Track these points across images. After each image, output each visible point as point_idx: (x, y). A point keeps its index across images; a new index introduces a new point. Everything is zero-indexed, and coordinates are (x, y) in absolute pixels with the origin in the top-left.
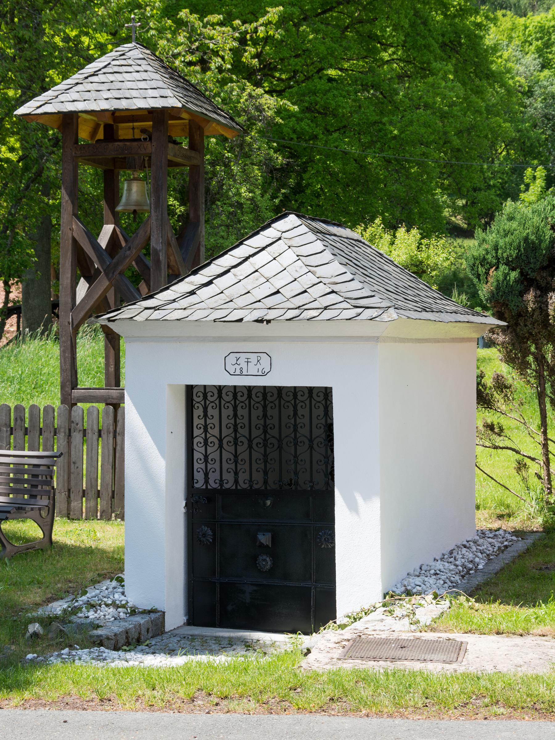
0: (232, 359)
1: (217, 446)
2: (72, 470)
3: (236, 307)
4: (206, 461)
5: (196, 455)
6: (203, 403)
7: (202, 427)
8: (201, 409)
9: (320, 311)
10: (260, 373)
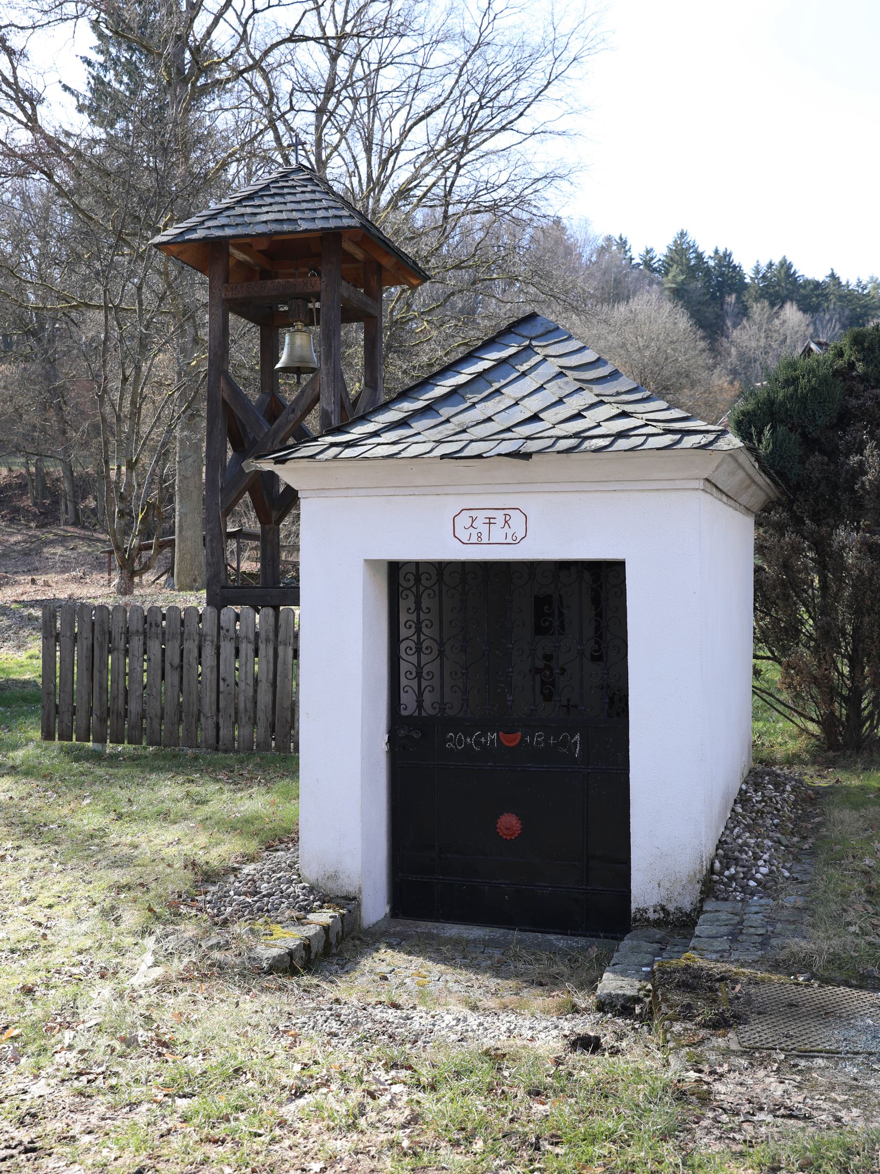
0: (464, 520)
1: (435, 653)
2: (221, 689)
3: (473, 438)
4: (419, 675)
5: (404, 667)
6: (414, 589)
7: (414, 626)
8: (412, 599)
9: (610, 440)
10: (509, 540)
